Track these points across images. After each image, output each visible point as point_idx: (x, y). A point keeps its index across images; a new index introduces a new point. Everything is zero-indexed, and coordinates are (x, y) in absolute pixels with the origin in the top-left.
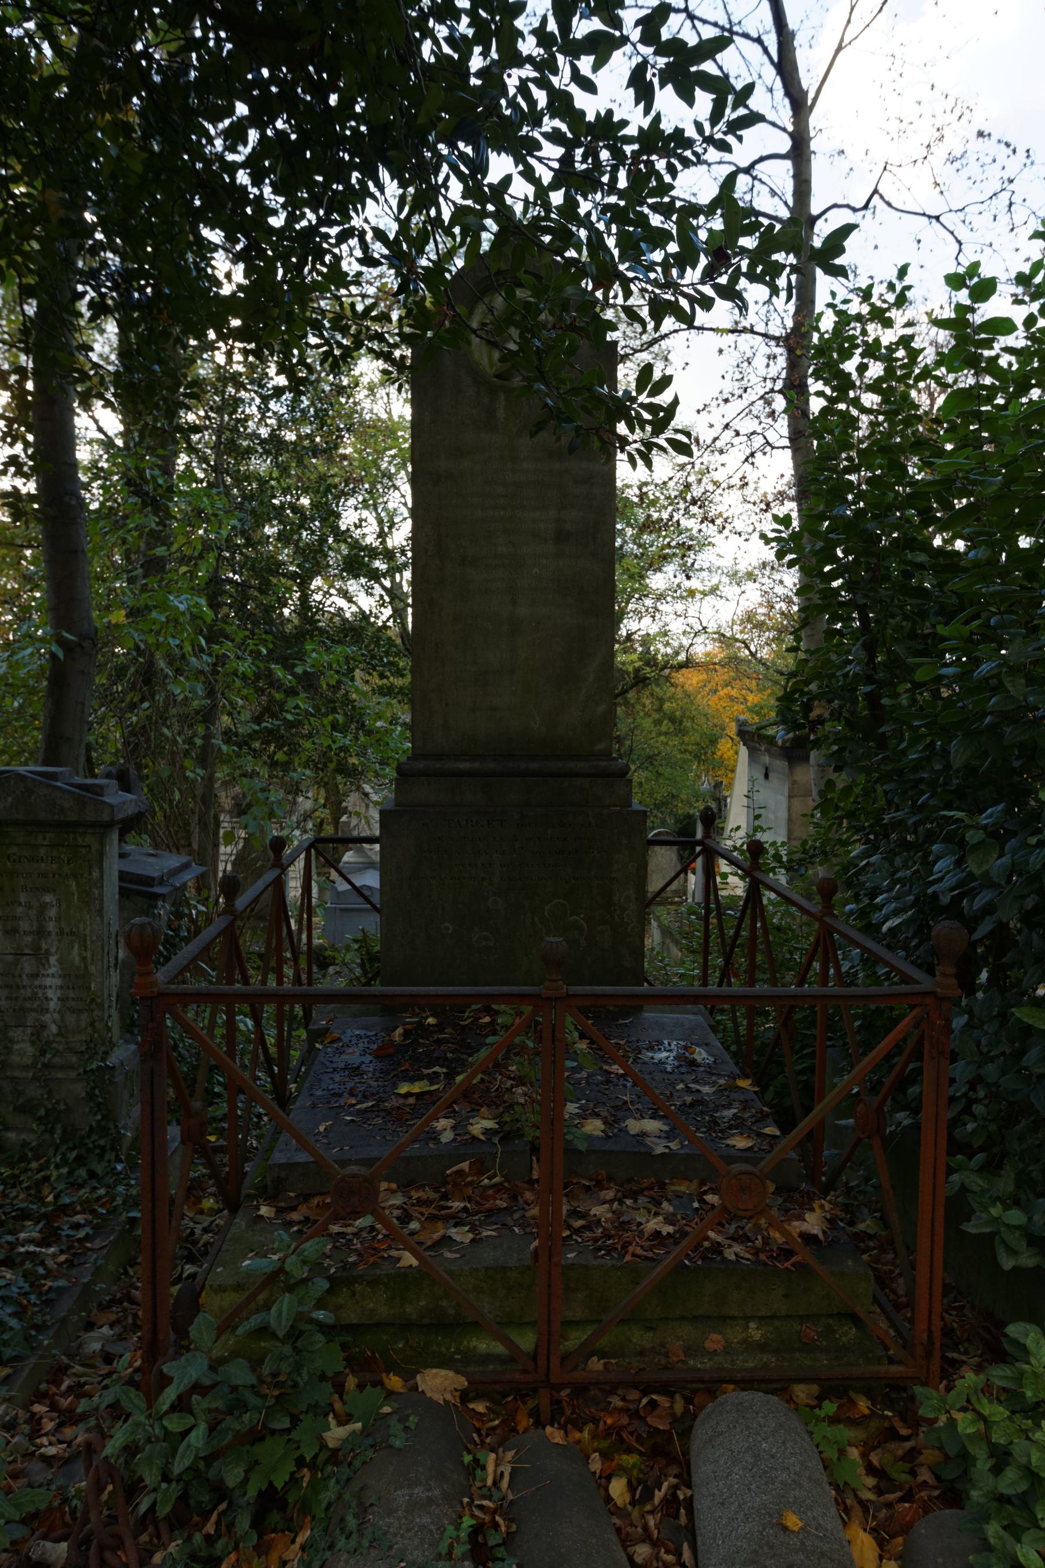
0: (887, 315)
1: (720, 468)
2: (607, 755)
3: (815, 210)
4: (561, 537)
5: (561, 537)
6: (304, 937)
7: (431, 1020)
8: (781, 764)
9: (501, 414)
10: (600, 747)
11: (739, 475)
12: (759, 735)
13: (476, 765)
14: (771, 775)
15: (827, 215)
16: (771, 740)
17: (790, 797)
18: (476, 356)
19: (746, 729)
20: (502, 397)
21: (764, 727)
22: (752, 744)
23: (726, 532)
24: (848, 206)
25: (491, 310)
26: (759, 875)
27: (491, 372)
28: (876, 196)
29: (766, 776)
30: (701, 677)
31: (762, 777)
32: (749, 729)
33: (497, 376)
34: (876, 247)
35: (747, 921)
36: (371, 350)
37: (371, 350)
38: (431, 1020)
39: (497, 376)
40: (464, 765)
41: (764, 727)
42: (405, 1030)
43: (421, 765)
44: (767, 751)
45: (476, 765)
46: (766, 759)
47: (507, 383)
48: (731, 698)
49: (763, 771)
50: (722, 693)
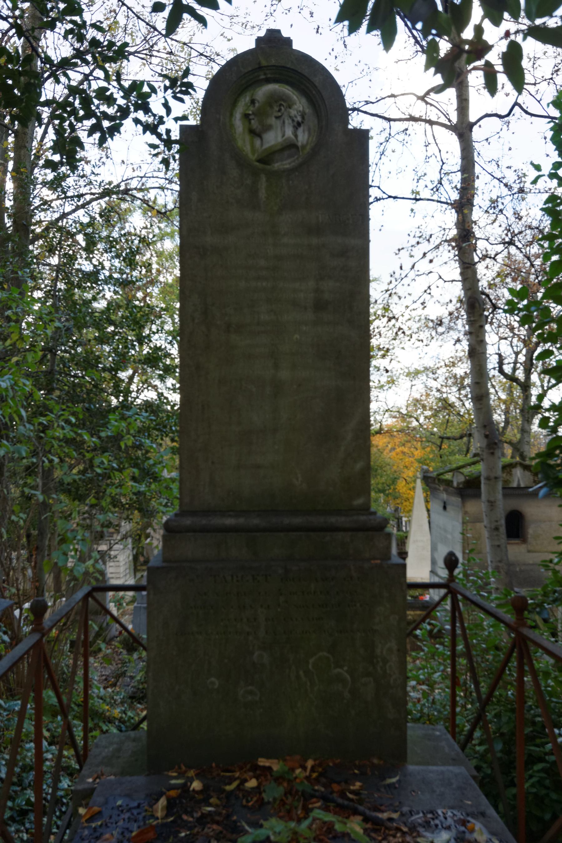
0: (178, 496)
1: (407, 296)
2: (366, 509)
3: (472, 119)
4: (320, 306)
5: (320, 306)
6: (80, 673)
7: (196, 785)
8: (457, 500)
9: (263, 194)
10: (359, 501)
11: (421, 300)
12: (439, 480)
13: (241, 521)
14: (448, 507)
15: (481, 123)
16: (449, 483)
17: (463, 523)
18: (240, 143)
19: (429, 475)
20: (263, 178)
21: (442, 474)
22: (433, 485)
23: (413, 340)
24: (496, 115)
25: (253, 102)
26: (526, 631)
27: (253, 157)
28: (517, 108)
29: (445, 508)
30: (385, 440)
31: (441, 508)
32: (431, 475)
33: (259, 161)
34: (510, 149)
35: (511, 674)
36: (137, 121)
37: (137, 121)
38: (196, 785)
39: (259, 161)
40: (229, 521)
41: (442, 474)
42: (169, 800)
43: (188, 521)
44: (445, 490)
45: (241, 521)
46: (444, 496)
47: (268, 167)
48: (403, 453)
49: (442, 505)
50: (398, 450)
